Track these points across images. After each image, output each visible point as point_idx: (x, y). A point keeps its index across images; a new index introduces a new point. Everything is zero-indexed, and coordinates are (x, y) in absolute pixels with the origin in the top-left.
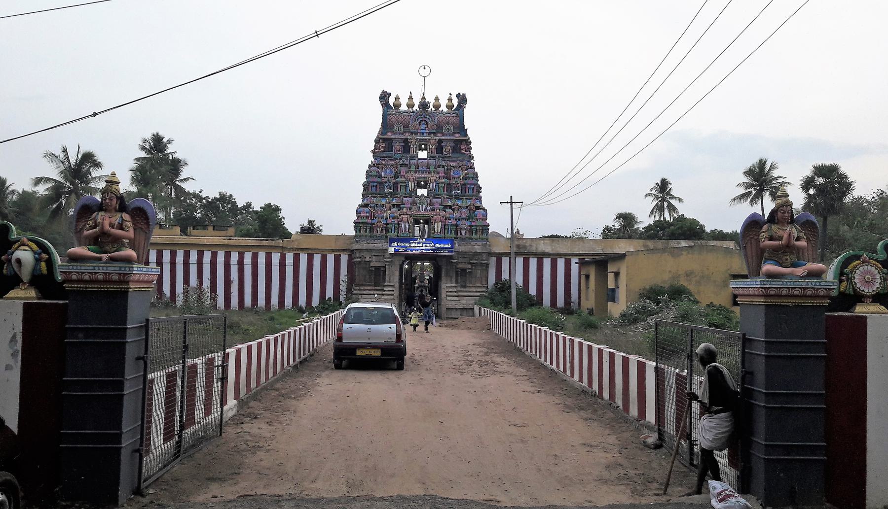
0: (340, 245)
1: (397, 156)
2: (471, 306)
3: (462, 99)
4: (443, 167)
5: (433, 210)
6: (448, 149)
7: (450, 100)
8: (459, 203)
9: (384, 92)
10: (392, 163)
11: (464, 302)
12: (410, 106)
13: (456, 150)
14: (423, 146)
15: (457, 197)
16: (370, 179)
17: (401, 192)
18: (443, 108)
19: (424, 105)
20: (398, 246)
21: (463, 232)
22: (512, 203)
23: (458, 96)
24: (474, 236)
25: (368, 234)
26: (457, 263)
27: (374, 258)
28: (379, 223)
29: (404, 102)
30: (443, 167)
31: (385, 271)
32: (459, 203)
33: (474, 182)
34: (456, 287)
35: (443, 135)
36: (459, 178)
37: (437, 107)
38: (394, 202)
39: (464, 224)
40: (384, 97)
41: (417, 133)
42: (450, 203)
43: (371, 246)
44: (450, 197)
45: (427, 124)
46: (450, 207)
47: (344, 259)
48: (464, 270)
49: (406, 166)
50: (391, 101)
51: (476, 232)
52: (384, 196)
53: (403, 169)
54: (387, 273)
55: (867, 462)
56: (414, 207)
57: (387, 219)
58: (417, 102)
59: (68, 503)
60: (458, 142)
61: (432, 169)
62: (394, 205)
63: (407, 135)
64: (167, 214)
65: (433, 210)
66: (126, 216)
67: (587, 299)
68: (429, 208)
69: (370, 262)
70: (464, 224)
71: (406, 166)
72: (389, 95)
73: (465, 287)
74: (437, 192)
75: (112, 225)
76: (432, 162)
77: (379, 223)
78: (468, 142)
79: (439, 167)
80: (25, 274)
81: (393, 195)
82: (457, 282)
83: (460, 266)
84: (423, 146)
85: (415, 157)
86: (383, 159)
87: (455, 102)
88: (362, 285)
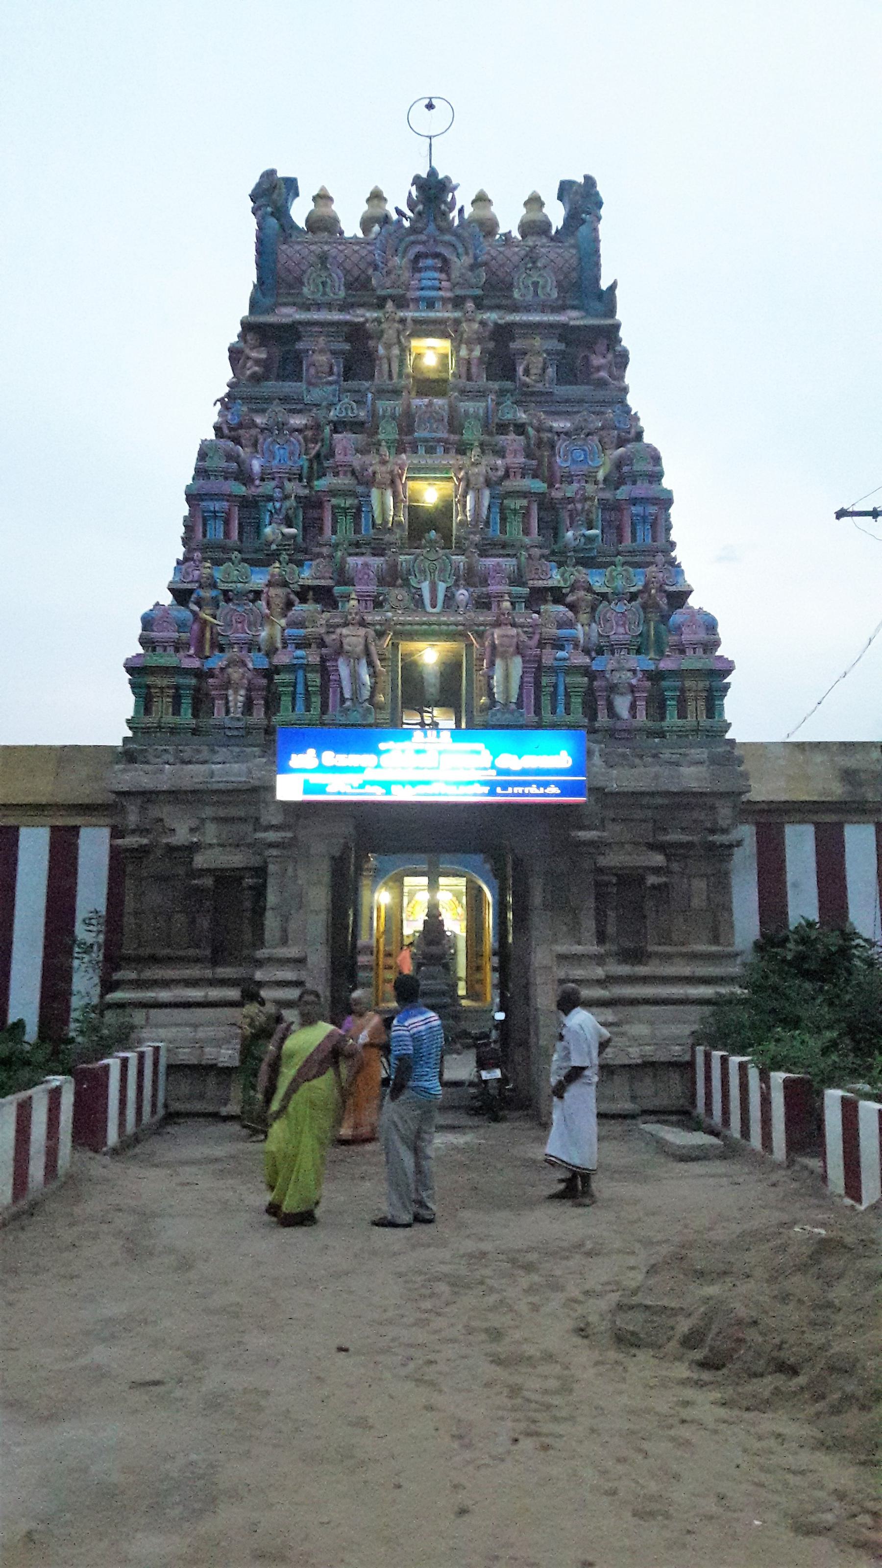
0: (77, 787)
1: (316, 395)
2: (676, 1051)
3: (583, 199)
4: (520, 429)
5: (483, 603)
6: (535, 360)
8: (598, 580)
9: (270, 175)
10: (297, 421)
11: (640, 1030)
13: (570, 370)
17: (335, 533)
20: (321, 768)
21: (622, 704)
23: (565, 190)
24: (672, 720)
25: (186, 717)
26: (597, 846)
27: (211, 833)
28: (239, 670)
30: (520, 429)
31: (260, 892)
32: (598, 580)
34: (600, 960)
36: (589, 477)
38: (307, 576)
39: (626, 668)
40: (271, 195)
41: (401, 302)
42: (555, 578)
43: (193, 775)
44: (559, 557)
45: (445, 267)
46: (557, 596)
47: (94, 848)
48: (629, 879)
49: (356, 426)
50: (300, 212)
51: (682, 703)
52: (263, 558)
53: (344, 441)
54: (272, 898)
55: (46, 857)
56: (398, 594)
57: (271, 652)
61: (472, 434)
62: (303, 594)
63: (360, 315)
65: (483, 603)
68: (462, 595)
69: (192, 848)
70: (626, 668)
71: (356, 426)
72: (291, 186)
73: (635, 956)
74: (495, 532)
77: (239, 670)
79: (502, 428)
81: (299, 553)
82: (601, 937)
83: (612, 859)
87: (556, 214)
88: (154, 960)
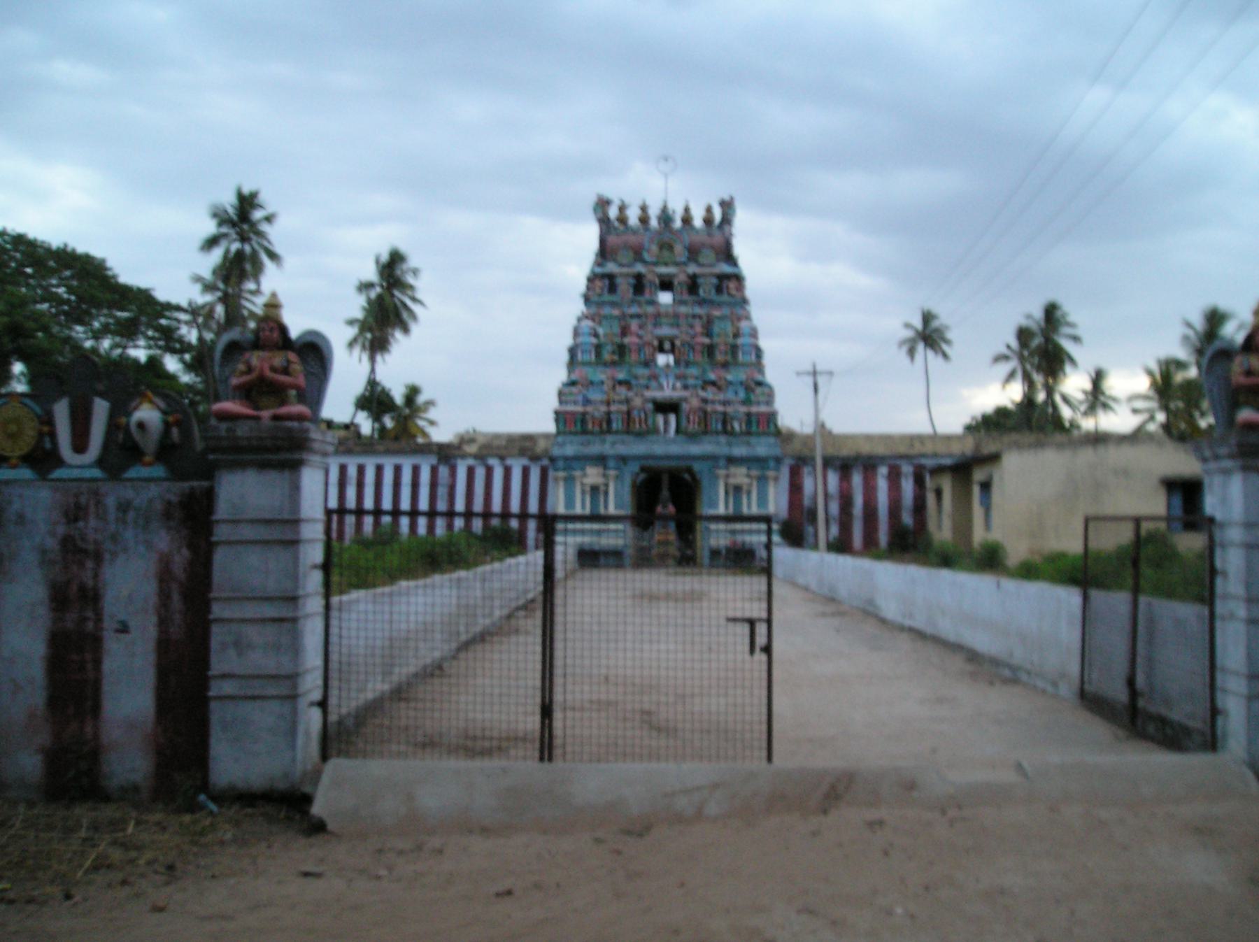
6: (706, 290)
7: (709, 210)
12: (644, 220)
14: (665, 289)
15: (725, 365)
16: (580, 340)
18: (698, 222)
19: (666, 218)
22: (815, 373)
29: (633, 216)
33: (752, 340)
35: (700, 265)
37: (687, 220)
38: (621, 376)
46: (713, 384)
50: (613, 213)
56: (654, 384)
58: (654, 213)
59: (211, 457)
60: (723, 278)
64: (695, 364)
66: (292, 356)
67: (940, 527)
75: (274, 369)
76: (683, 310)
78: (738, 278)
80: (150, 443)
84: (665, 289)
85: (653, 303)
86: (601, 304)
87: (717, 214)
